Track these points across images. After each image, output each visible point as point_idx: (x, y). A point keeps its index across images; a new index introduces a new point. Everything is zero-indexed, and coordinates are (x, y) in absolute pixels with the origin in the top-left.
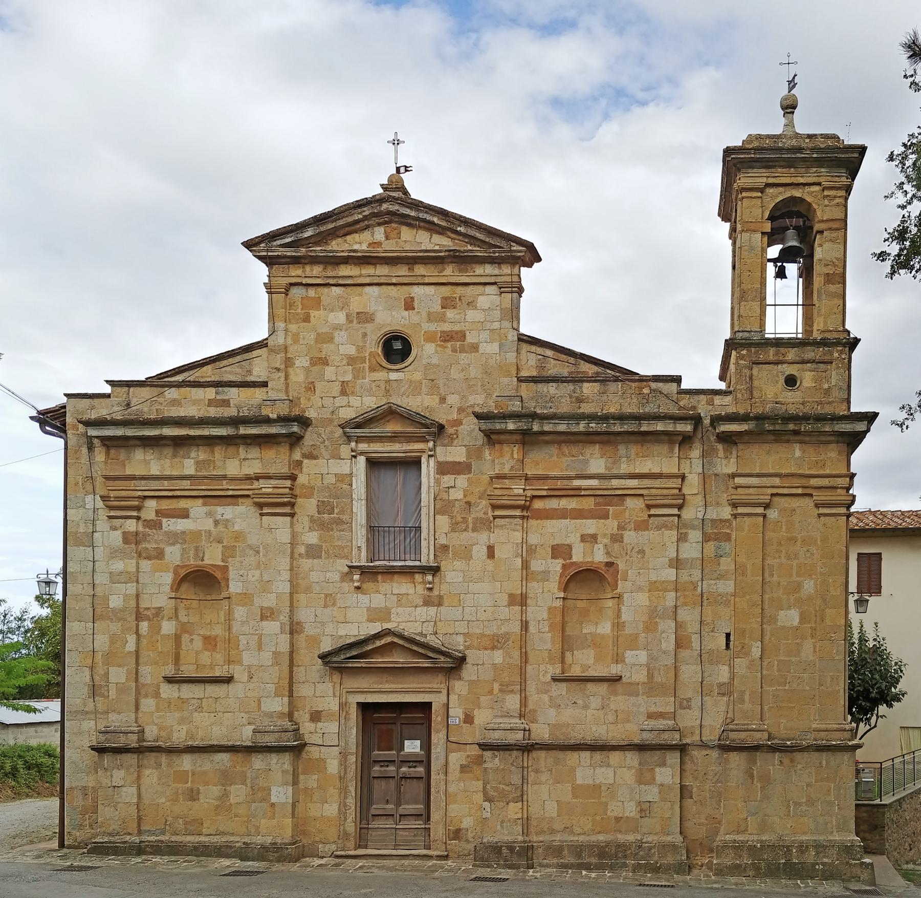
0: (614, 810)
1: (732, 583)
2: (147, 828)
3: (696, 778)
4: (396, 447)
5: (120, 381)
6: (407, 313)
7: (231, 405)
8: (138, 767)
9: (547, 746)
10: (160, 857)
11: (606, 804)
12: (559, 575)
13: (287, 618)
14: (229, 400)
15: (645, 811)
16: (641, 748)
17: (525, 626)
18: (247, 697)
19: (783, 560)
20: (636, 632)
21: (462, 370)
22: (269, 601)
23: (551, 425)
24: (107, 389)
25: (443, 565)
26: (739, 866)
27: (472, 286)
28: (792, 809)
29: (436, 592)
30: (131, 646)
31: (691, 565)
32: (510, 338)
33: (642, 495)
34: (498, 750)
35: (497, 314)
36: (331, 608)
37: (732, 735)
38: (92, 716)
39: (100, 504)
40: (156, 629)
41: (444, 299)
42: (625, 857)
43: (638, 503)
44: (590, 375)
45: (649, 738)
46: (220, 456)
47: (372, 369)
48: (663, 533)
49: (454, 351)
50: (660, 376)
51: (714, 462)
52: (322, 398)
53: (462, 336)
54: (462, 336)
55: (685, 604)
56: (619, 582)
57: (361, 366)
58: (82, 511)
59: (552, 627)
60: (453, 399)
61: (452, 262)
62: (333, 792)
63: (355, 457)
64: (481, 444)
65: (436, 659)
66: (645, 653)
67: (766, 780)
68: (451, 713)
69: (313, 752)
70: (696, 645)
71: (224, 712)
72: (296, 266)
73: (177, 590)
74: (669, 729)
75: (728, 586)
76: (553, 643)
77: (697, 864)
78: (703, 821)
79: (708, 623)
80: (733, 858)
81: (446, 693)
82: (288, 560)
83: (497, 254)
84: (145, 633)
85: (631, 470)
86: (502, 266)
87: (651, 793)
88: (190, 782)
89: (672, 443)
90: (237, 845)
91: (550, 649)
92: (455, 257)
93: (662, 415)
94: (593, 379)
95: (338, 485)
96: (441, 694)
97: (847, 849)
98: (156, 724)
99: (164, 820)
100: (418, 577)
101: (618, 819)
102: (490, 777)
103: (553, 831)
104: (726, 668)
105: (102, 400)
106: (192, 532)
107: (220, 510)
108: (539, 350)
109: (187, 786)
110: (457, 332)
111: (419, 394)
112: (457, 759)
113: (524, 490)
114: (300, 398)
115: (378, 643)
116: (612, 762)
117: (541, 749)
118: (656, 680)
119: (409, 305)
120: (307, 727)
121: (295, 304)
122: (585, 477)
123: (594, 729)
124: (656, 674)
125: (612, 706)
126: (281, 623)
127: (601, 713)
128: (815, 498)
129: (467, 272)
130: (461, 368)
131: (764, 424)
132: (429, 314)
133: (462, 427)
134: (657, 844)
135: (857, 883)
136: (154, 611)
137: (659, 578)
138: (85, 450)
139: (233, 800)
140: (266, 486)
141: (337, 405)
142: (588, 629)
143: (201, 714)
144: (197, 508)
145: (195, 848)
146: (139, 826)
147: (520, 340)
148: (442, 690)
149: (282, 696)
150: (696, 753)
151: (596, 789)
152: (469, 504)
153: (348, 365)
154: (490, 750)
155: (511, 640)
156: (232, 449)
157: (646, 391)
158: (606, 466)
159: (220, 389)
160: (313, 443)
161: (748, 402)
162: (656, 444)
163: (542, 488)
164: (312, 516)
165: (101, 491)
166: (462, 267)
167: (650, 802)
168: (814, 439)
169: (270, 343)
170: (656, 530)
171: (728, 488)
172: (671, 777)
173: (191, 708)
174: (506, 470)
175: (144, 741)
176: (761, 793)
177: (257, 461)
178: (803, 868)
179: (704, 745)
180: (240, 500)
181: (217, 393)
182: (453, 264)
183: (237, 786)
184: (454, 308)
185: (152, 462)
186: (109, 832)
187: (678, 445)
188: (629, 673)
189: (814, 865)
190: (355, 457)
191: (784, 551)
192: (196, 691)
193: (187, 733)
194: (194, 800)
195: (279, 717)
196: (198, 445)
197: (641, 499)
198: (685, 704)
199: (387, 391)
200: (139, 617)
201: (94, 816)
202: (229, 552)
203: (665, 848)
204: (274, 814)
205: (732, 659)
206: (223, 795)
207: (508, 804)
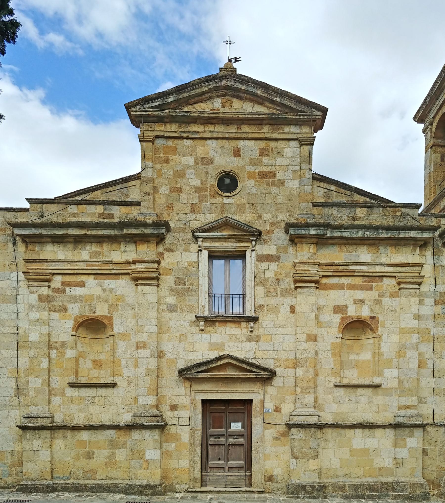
0: (378, 463)
2: (57, 475)
3: (430, 444)
4: (229, 245)
5: (37, 199)
6: (235, 159)
7: (115, 218)
8: (51, 438)
9: (334, 426)
10: (68, 493)
11: (372, 460)
13: (155, 348)
14: (113, 214)
15: (400, 464)
16: (396, 426)
17: (316, 353)
18: (126, 396)
20: (391, 358)
21: (273, 198)
22: (143, 337)
23: (339, 233)
24: (27, 205)
25: (260, 317)
27: (280, 141)
29: (255, 334)
30: (45, 364)
31: (427, 319)
32: (307, 176)
34: (302, 428)
35: (298, 160)
36: (184, 343)
38: (18, 408)
39: (21, 277)
40: (62, 354)
41: (261, 149)
42: (387, 491)
43: (391, 281)
44: (361, 202)
45: (400, 420)
46: (107, 249)
47: (212, 196)
48: (409, 299)
49: (268, 185)
51: (441, 258)
52: (178, 214)
53: (273, 175)
54: (273, 175)
55: (423, 341)
56: (379, 328)
57: (205, 193)
58: (8, 282)
59: (334, 355)
60: (267, 217)
61: (268, 124)
62: (186, 454)
63: (201, 251)
64: (287, 244)
65: (258, 373)
66: (397, 370)
68: (265, 406)
69: (172, 429)
70: (430, 365)
71: (110, 405)
72: (160, 124)
73: (76, 331)
74: (416, 415)
78: (435, 469)
81: (263, 394)
82: (156, 313)
83: (301, 117)
84: (54, 357)
85: (388, 261)
86: (302, 127)
87: (403, 453)
88: (87, 448)
89: (415, 246)
90: (122, 485)
91: (333, 368)
92: (272, 119)
93: (416, 227)
94: (364, 205)
95: (189, 268)
96: (259, 394)
98: (62, 413)
99: (69, 471)
100: (243, 324)
101: (380, 469)
102: (296, 444)
105: (22, 213)
106: (87, 296)
107: (106, 282)
108: (326, 186)
109: (85, 450)
110: (269, 173)
111: (244, 213)
112: (270, 433)
113: (317, 271)
114: (163, 214)
115: (219, 363)
116: (376, 435)
117: (329, 427)
118: (405, 386)
119: (237, 153)
120: (168, 414)
121: (159, 151)
124: (405, 383)
126: (151, 351)
129: (278, 130)
130: (272, 196)
132: (251, 159)
133: (273, 235)
136: (60, 344)
137: (407, 326)
138: (10, 245)
139: (117, 458)
140: (140, 267)
141: (188, 219)
143: (94, 406)
144: (90, 281)
145: (93, 488)
146: (52, 474)
147: (314, 178)
148: (260, 392)
149: (152, 395)
150: (430, 429)
151: (366, 451)
152: (278, 280)
153: (196, 192)
154: (296, 427)
155: (308, 361)
156: (115, 245)
157: (398, 214)
158: (371, 258)
159: (107, 206)
160: (172, 242)
162: (404, 246)
164: (171, 287)
165: (22, 267)
166: (275, 127)
167: (403, 458)
169: (143, 176)
170: (405, 297)
172: (417, 443)
173: (87, 402)
174: (305, 259)
175: (54, 422)
177: (133, 252)
180: (121, 276)
181: (105, 209)
182: (269, 125)
183: (120, 450)
184: (268, 156)
185: (59, 253)
186: (30, 478)
187: (418, 247)
190: (201, 251)
192: (92, 392)
193: (85, 417)
194: (90, 458)
195: (150, 408)
196: (91, 242)
197: (394, 279)
198: (422, 401)
199: (222, 211)
200: (50, 347)
201: (19, 469)
202: (113, 307)
203: (414, 485)
204: (148, 466)
206: (111, 455)
207: (308, 460)
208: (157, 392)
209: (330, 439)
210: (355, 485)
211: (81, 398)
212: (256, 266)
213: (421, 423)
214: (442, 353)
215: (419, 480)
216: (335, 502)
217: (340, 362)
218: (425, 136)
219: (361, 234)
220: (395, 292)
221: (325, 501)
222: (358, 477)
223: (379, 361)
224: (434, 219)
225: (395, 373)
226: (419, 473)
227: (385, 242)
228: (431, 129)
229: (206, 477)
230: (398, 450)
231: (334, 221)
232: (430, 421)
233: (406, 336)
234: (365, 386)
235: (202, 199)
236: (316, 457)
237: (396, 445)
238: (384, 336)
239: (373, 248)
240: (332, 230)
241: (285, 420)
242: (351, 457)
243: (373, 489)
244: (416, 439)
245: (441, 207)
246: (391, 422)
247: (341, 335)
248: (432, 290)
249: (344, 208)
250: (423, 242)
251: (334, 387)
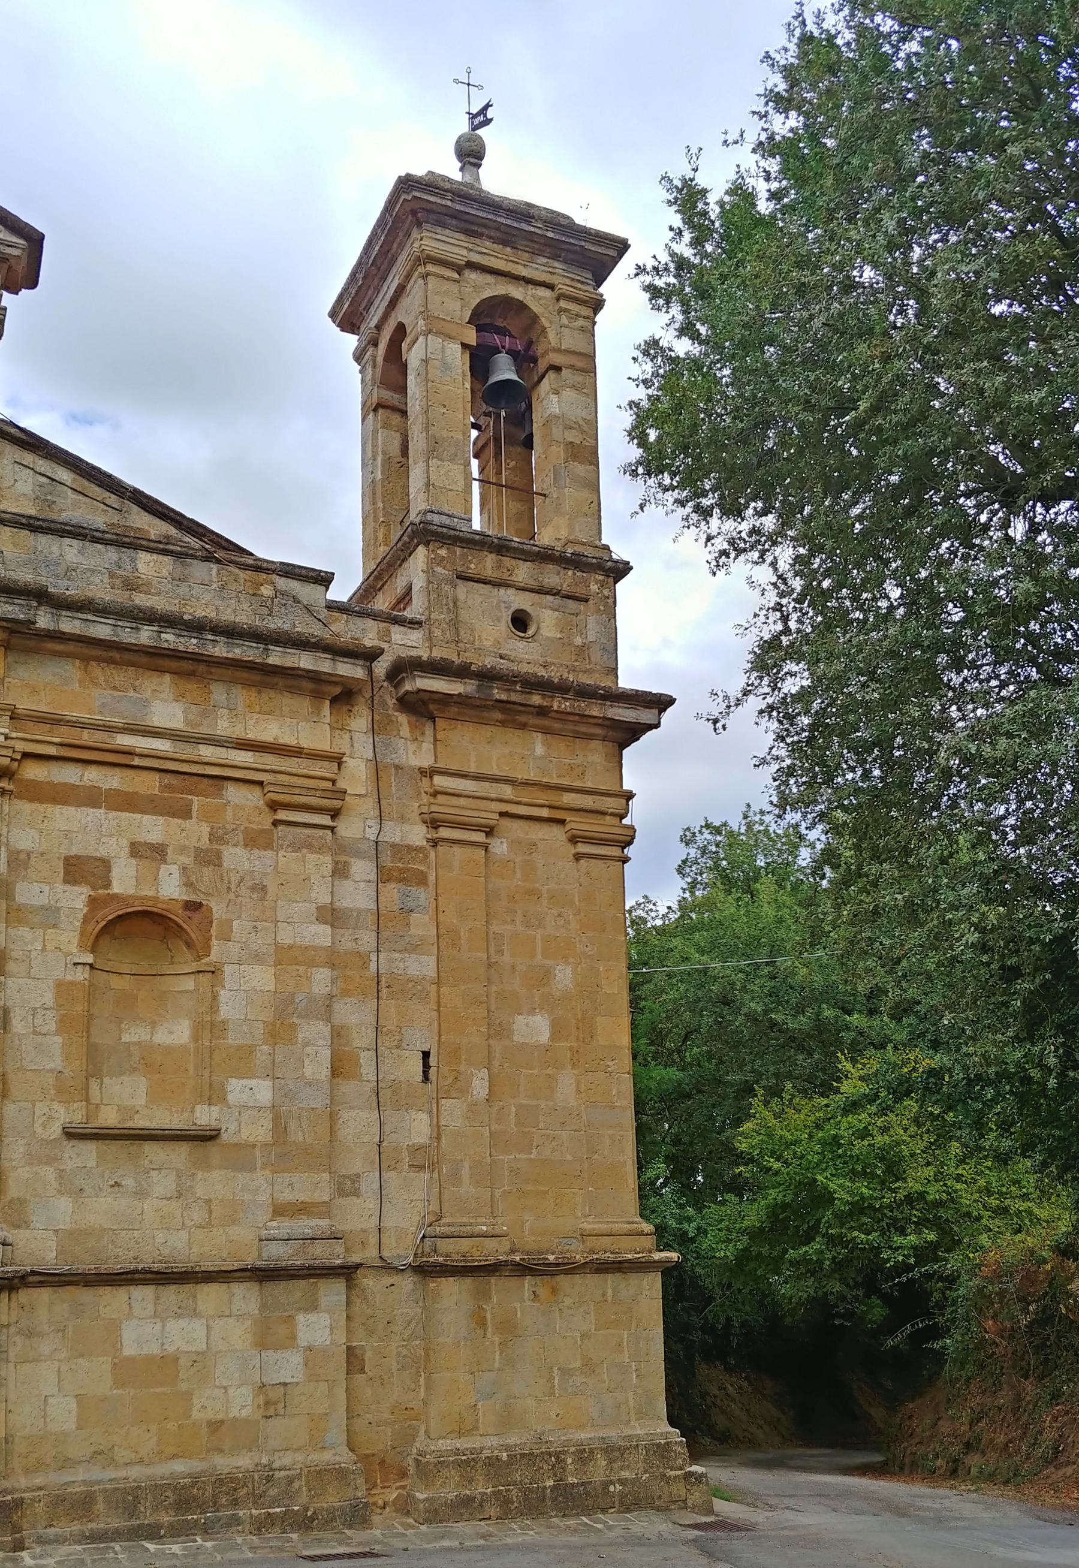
1: (432, 960)
3: (371, 1333)
9: (57, 1279)
11: (188, 1396)
12: (80, 916)
15: (275, 1403)
19: (519, 927)
23: (77, 623)
26: (471, 1499)
28: (556, 1381)
33: (261, 783)
37: (444, 1245)
43: (250, 796)
44: (153, 537)
45: (279, 1253)
48: (304, 857)
50: (294, 566)
55: (346, 993)
56: (214, 942)
59: (65, 1025)
66: (268, 1083)
67: (509, 1328)
70: (367, 1070)
75: (423, 966)
76: (67, 1057)
77: (374, 1504)
78: (387, 1416)
79: (390, 1032)
80: (457, 1486)
85: (237, 731)
89: (317, 696)
91: (60, 1068)
93: (313, 640)
94: (161, 546)
97: (662, 1451)
101: (215, 1426)
103: (66, 1463)
104: (424, 1117)
108: (43, 465)
113: (7, 738)
116: (201, 1306)
117: (41, 1284)
118: (292, 1138)
122: (145, 731)
123: (160, 1237)
124: (293, 1126)
125: (200, 1191)
127: (175, 1206)
128: (568, 827)
131: (492, 688)
134: (306, 1470)
135: (683, 1512)
142: (134, 1034)
150: (371, 1283)
157: (266, 591)
158: (186, 718)
161: (453, 646)
163: (49, 740)
167: (285, 1384)
168: (570, 727)
171: (420, 794)
176: (501, 1354)
178: (587, 1494)
179: (387, 1267)
188: (236, 1123)
189: (605, 1485)
191: (519, 912)
197: (257, 791)
203: (320, 1475)
205: (435, 1101)
209: (46, 1327)
213: (338, 1262)
214: (403, 1030)
215: (337, 1458)
216: (51, 1561)
217: (85, 1049)
218: (361, 372)
219: (149, 638)
220: (262, 831)
221: (14, 1560)
222: (141, 1461)
223: (212, 1051)
224: (370, 623)
225: (263, 1091)
226: (337, 1434)
227: (229, 673)
228: (374, 358)
230: (270, 1355)
231: (66, 583)
232: (369, 1254)
233: (294, 974)
234: (163, 1136)
237: (264, 1341)
238: (228, 969)
239: (189, 686)
240: (54, 611)
242: (117, 1388)
243: (187, 1501)
244: (326, 1316)
245: (399, 590)
246: (251, 1261)
247: (89, 958)
249: (99, 546)
250: (337, 690)
251: (64, 1137)
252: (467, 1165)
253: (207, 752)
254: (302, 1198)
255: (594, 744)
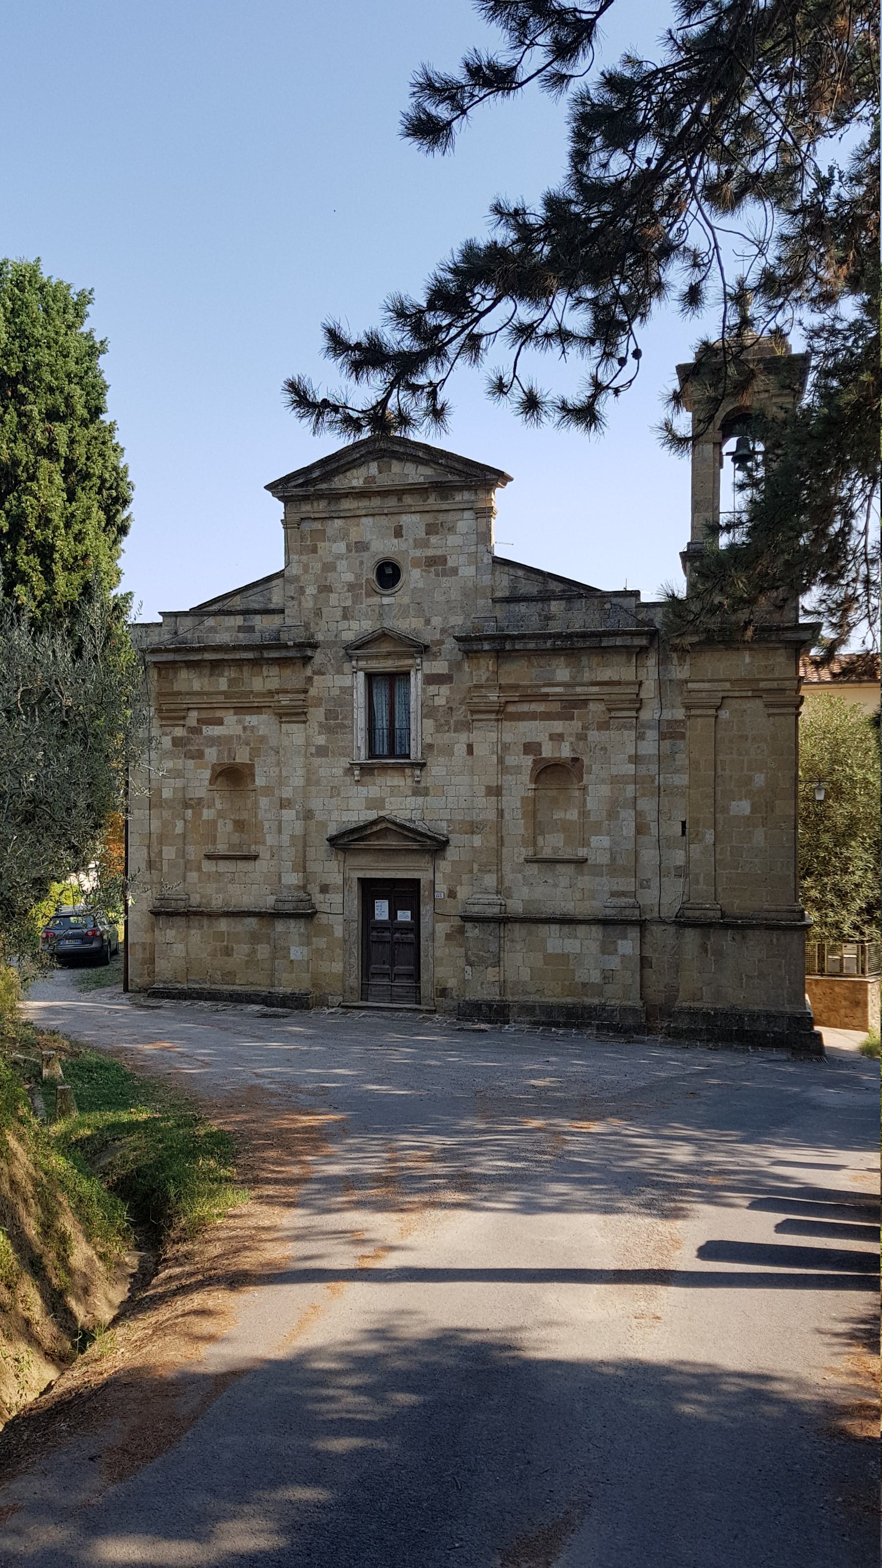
0: (581, 976)
1: (686, 777)
11: (573, 971)
16: (605, 923)
17: (501, 813)
21: (444, 593)
22: (287, 793)
24: (160, 619)
29: (423, 784)
32: (485, 561)
40: (198, 815)
47: (368, 595)
49: (437, 575)
53: (443, 560)
54: (443, 560)
55: (643, 795)
56: (585, 775)
59: (524, 815)
60: (436, 621)
67: (719, 954)
68: (436, 889)
69: (323, 919)
70: (654, 831)
76: (526, 829)
87: (614, 962)
90: (263, 993)
101: (584, 985)
102: (471, 945)
104: (682, 852)
106: (225, 736)
108: (512, 571)
111: (407, 617)
112: (442, 928)
116: (578, 935)
119: (398, 533)
120: (318, 897)
124: (618, 856)
132: (415, 540)
141: (340, 629)
142: (558, 815)
144: (230, 718)
151: (564, 957)
152: (451, 709)
154: (471, 921)
157: (608, 606)
169: (286, 574)
179: (662, 921)
180: (264, 710)
187: (634, 656)
198: (644, 884)
202: (255, 752)
203: (625, 1010)
208: (305, 867)
210: (547, 1007)
211: (220, 874)
212: (424, 690)
220: (605, 722)
226: (635, 993)
229: (366, 987)
235: (356, 599)
236: (497, 963)
237: (604, 951)
241: (460, 911)
247: (533, 786)
248: (656, 717)
252: (702, 876)
253: (579, 689)
254: (622, 889)
255: (780, 652)
